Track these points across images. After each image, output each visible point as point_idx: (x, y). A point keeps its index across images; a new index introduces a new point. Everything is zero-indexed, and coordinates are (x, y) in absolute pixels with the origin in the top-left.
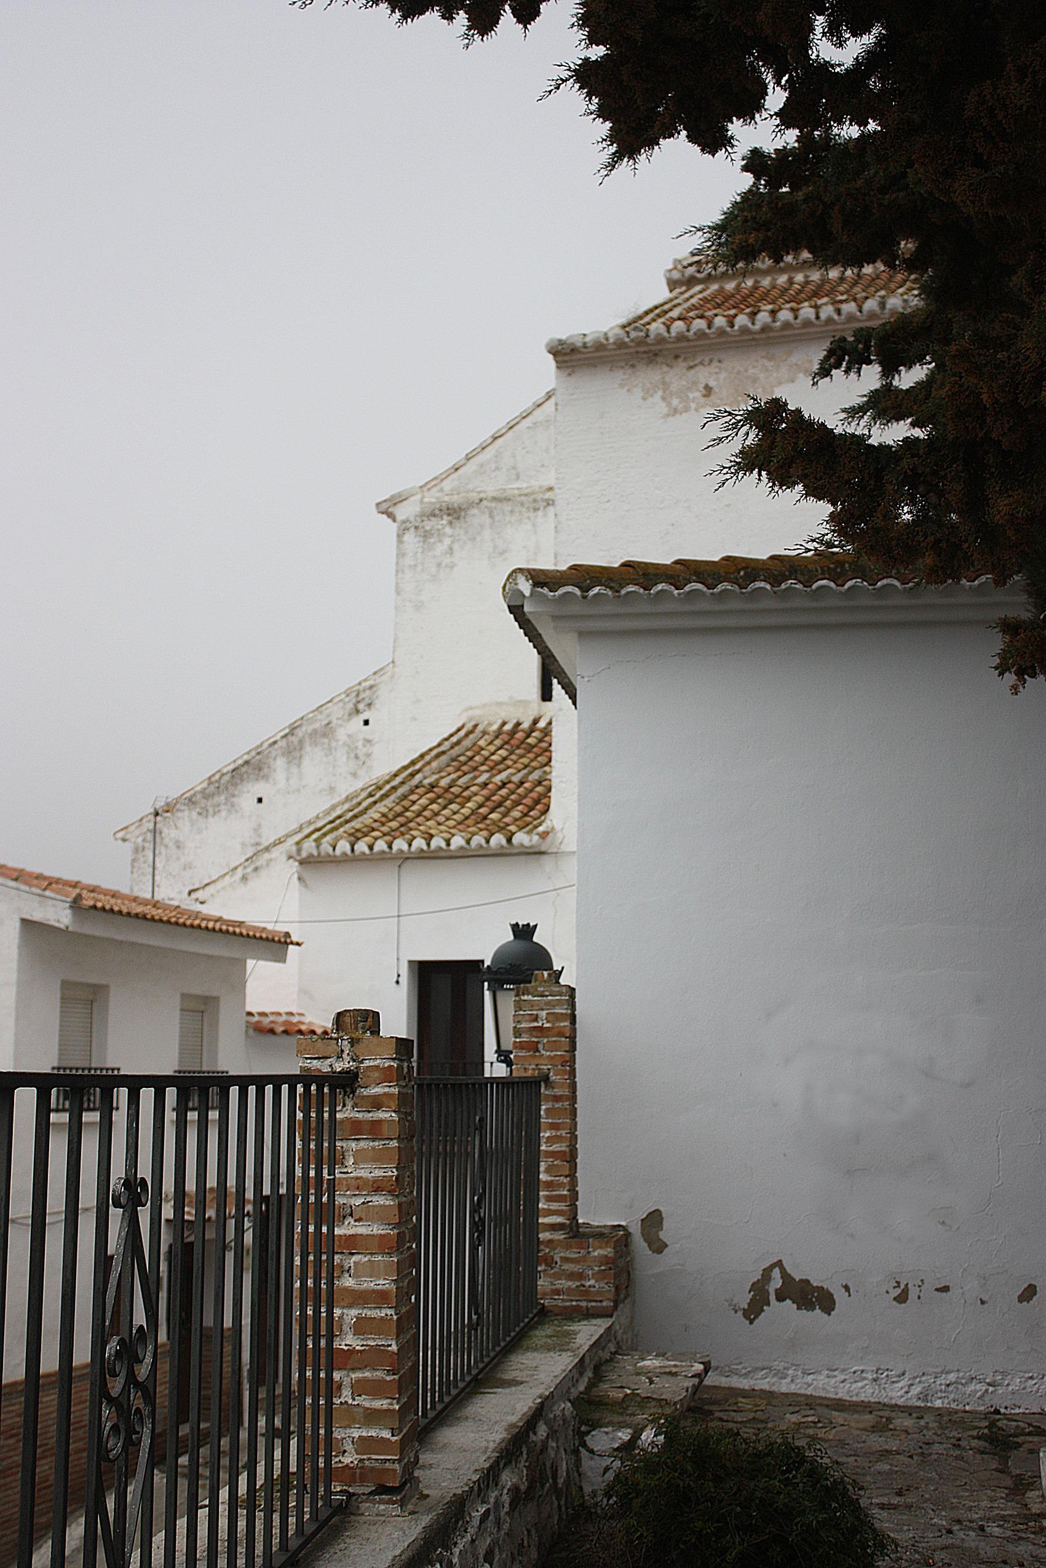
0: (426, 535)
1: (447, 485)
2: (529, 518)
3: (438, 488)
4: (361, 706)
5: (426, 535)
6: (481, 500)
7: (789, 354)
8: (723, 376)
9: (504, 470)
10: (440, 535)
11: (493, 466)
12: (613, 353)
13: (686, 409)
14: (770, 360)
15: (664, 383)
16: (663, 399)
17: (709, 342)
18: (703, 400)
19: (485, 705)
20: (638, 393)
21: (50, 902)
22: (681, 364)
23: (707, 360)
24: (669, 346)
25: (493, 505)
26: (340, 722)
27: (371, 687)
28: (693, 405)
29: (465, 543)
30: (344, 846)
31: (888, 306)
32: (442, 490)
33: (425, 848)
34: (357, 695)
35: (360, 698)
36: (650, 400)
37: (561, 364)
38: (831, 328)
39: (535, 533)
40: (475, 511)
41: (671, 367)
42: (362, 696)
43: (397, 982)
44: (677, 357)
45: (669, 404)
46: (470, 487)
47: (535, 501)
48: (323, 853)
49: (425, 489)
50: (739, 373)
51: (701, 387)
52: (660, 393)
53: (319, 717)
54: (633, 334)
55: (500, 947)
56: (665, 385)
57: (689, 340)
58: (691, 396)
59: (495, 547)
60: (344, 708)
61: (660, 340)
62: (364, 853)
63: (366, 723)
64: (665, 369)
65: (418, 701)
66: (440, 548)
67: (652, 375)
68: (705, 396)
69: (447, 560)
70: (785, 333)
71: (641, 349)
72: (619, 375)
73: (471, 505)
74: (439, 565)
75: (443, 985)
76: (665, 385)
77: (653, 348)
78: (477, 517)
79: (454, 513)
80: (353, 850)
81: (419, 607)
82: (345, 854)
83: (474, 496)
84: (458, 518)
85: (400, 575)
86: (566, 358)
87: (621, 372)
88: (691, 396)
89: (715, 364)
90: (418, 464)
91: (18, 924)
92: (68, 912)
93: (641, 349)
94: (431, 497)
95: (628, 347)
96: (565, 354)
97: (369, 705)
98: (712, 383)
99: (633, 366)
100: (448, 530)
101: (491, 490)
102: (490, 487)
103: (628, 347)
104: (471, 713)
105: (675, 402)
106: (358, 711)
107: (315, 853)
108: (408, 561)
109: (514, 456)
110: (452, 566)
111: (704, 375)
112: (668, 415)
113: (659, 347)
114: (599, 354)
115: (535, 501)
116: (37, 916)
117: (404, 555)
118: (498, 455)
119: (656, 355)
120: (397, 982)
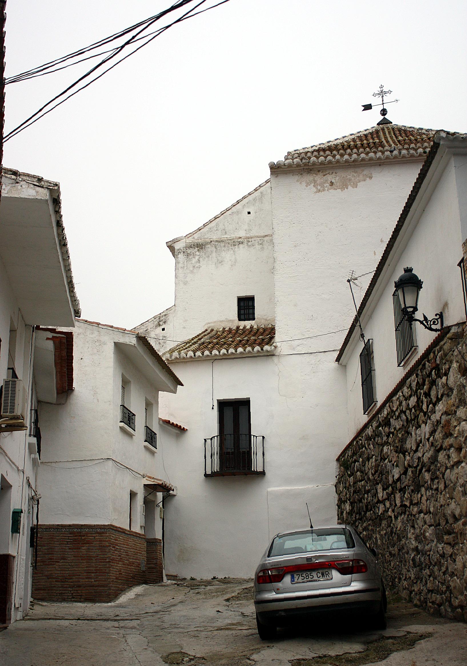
0: (188, 255)
1: (196, 236)
2: (232, 249)
3: (192, 237)
4: (161, 323)
5: (188, 255)
6: (211, 241)
7: (363, 171)
8: (338, 178)
9: (220, 231)
10: (194, 255)
11: (215, 229)
12: (294, 169)
13: (324, 190)
14: (355, 173)
15: (314, 180)
16: (314, 186)
17: (332, 165)
18: (330, 187)
19: (215, 322)
20: (304, 184)
21: (128, 335)
22: (321, 174)
23: (331, 172)
24: (316, 167)
25: (217, 243)
26: (152, 329)
27: (165, 315)
28: (326, 189)
29: (205, 258)
30: (191, 354)
31: (402, 153)
32: (194, 238)
33: (226, 353)
34: (159, 319)
35: (161, 319)
36: (309, 187)
37: (272, 173)
38: (379, 161)
39: (235, 254)
40: (209, 246)
41: (317, 175)
42: (161, 319)
43: (213, 408)
44: (319, 171)
45: (317, 188)
46: (206, 237)
47: (234, 242)
48: (181, 357)
49: (186, 237)
50: (344, 177)
51: (329, 182)
52: (313, 184)
53: (143, 327)
54: (304, 161)
55: (400, 277)
56: (315, 182)
57: (325, 165)
58: (325, 185)
59: (218, 260)
60: (153, 324)
61: (314, 164)
62: (199, 356)
63: (163, 329)
64: (314, 175)
65: (186, 321)
66: (194, 260)
67: (310, 178)
68: (330, 185)
69: (198, 265)
70: (362, 163)
71: (305, 167)
72: (296, 177)
73: (207, 243)
74: (194, 267)
75: (229, 413)
76: (315, 182)
77: (310, 167)
78: (210, 248)
79: (200, 246)
80: (195, 355)
81: (185, 283)
82: (191, 357)
83: (209, 241)
84: (202, 248)
85: (177, 271)
86: (276, 170)
87: (297, 176)
88: (325, 185)
89: (334, 174)
90: (185, 225)
91: (113, 344)
92: (135, 339)
93: (305, 167)
94: (190, 240)
95: (301, 166)
96: (276, 169)
97: (165, 322)
98: (333, 181)
99: (301, 174)
100: (198, 253)
101: (215, 238)
102: (215, 237)
103: (301, 166)
104: (209, 325)
105: (319, 187)
106: (160, 325)
107: (178, 357)
108: (180, 265)
109: (224, 225)
110: (199, 267)
111: (330, 178)
112: (316, 192)
113: (312, 167)
114: (290, 169)
115: (234, 242)
116: (121, 341)
117: (179, 263)
118: (217, 225)
119: (311, 170)
120: (213, 408)
